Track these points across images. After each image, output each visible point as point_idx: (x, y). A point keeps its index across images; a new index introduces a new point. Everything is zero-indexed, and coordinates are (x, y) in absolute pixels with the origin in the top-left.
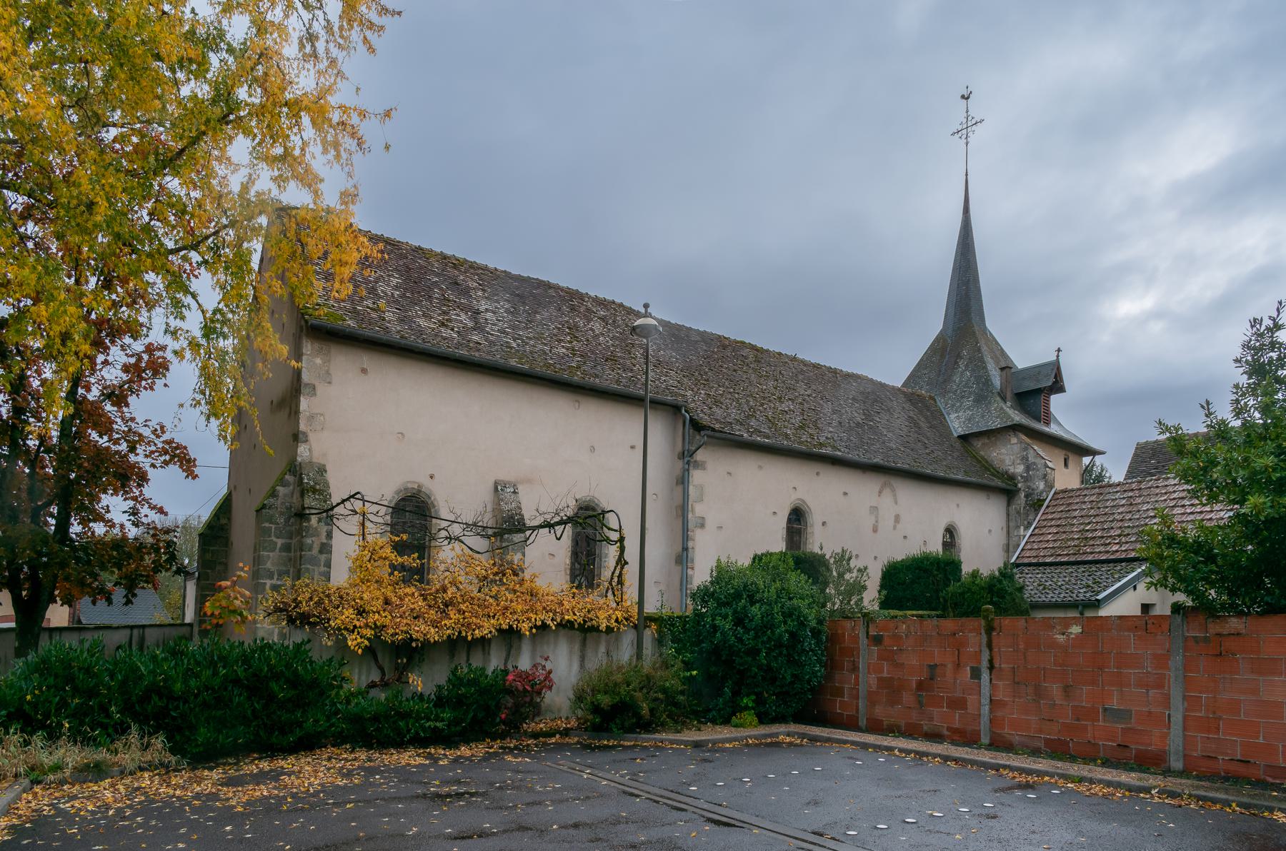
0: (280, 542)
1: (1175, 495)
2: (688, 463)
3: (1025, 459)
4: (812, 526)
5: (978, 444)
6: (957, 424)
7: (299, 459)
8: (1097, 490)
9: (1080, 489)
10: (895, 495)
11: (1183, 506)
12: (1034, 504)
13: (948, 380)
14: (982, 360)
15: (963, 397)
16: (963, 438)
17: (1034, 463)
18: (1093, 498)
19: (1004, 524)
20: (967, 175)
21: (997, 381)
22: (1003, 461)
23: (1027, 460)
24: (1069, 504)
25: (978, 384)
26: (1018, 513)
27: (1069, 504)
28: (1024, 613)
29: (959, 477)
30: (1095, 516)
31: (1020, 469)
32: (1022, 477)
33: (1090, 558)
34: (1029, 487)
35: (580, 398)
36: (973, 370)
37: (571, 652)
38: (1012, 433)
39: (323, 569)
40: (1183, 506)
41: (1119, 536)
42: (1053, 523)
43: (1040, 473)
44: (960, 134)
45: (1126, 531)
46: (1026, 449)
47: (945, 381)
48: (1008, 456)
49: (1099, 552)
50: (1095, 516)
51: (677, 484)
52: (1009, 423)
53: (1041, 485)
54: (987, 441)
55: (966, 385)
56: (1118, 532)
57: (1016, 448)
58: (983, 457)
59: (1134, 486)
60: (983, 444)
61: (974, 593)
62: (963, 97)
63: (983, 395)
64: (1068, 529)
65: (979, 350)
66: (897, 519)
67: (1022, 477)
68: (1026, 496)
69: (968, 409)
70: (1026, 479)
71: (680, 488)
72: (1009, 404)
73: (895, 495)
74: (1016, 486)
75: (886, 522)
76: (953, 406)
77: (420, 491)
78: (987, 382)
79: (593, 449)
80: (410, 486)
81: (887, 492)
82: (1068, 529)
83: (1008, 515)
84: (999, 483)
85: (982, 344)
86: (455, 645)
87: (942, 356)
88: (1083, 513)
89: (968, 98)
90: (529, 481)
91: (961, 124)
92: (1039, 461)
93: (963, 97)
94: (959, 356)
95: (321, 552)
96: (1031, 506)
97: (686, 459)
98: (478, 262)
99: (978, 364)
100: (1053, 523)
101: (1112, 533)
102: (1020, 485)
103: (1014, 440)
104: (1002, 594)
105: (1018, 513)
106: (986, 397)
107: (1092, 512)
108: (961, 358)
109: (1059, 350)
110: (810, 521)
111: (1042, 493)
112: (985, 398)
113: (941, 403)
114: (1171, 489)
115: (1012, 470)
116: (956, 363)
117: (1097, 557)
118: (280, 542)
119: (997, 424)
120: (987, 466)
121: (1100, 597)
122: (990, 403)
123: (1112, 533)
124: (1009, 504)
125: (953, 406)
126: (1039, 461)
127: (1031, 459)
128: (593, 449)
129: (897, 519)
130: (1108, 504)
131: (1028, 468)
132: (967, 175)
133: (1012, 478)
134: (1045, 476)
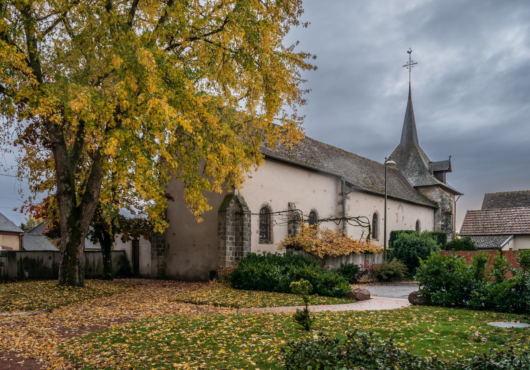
0: (231, 222)
1: (515, 215)
2: (345, 197)
3: (441, 197)
4: (379, 220)
5: (421, 190)
6: (412, 181)
7: (235, 194)
8: (485, 212)
9: (481, 211)
10: (403, 209)
11: (518, 218)
12: (445, 213)
13: (405, 164)
14: (420, 158)
15: (413, 172)
16: (416, 188)
17: (445, 199)
18: (484, 214)
19: (433, 220)
20: (410, 84)
21: (427, 166)
22: (432, 197)
23: (442, 197)
24: (475, 216)
25: (419, 167)
26: (439, 216)
27: (475, 216)
28: (476, 250)
29: (422, 203)
30: (486, 220)
31: (439, 200)
32: (440, 203)
33: (489, 234)
34: (443, 207)
35: (311, 174)
36: (416, 162)
37: (362, 260)
38: (436, 187)
39: (249, 232)
40: (518, 218)
41: (498, 227)
42: (471, 222)
43: (448, 202)
44: (407, 67)
45: (500, 226)
46: (442, 193)
47: (404, 165)
48: (435, 195)
49: (491, 232)
50: (486, 220)
51: (339, 204)
52: (436, 184)
53: (448, 207)
54: (425, 189)
55: (414, 167)
56: (497, 226)
57: (438, 193)
58: (424, 195)
59: (499, 211)
60: (424, 190)
61: (459, 244)
62: (408, 52)
63: (422, 172)
64: (477, 224)
65: (418, 154)
66: (403, 217)
67: (440, 203)
68: (442, 210)
69: (416, 176)
70: (442, 204)
71: (340, 207)
72: (433, 176)
73: (403, 209)
74: (438, 206)
75: (400, 219)
76: (409, 175)
77: (267, 206)
78: (424, 166)
79: (314, 191)
80: (265, 204)
81: (400, 208)
82: (477, 224)
83: (434, 217)
84: (432, 205)
85: (419, 151)
86: (341, 256)
87: (402, 154)
88: (482, 219)
89: (410, 53)
90: (297, 203)
91: (407, 63)
92: (447, 198)
93: (408, 52)
94: (409, 155)
95: (248, 226)
96: (444, 214)
97: (344, 196)
98: (494, 193)
99: (418, 159)
100: (471, 222)
101: (494, 226)
102: (439, 206)
103: (437, 190)
104: (468, 245)
105: (439, 216)
106: (424, 173)
107: (485, 219)
108: (411, 156)
109: (450, 156)
110: (379, 218)
111: (448, 209)
112: (423, 173)
113: (403, 173)
114: (513, 213)
115: (436, 200)
116: (408, 158)
117: (491, 234)
118: (231, 222)
119: (430, 183)
120: (426, 199)
121: (501, 246)
122: (425, 175)
123: (494, 226)
124: (435, 213)
125: (409, 175)
126: (447, 198)
127: (444, 197)
128: (314, 191)
129: (403, 217)
130: (490, 216)
131: (443, 200)
132: (410, 84)
133: (436, 203)
134: (450, 203)
